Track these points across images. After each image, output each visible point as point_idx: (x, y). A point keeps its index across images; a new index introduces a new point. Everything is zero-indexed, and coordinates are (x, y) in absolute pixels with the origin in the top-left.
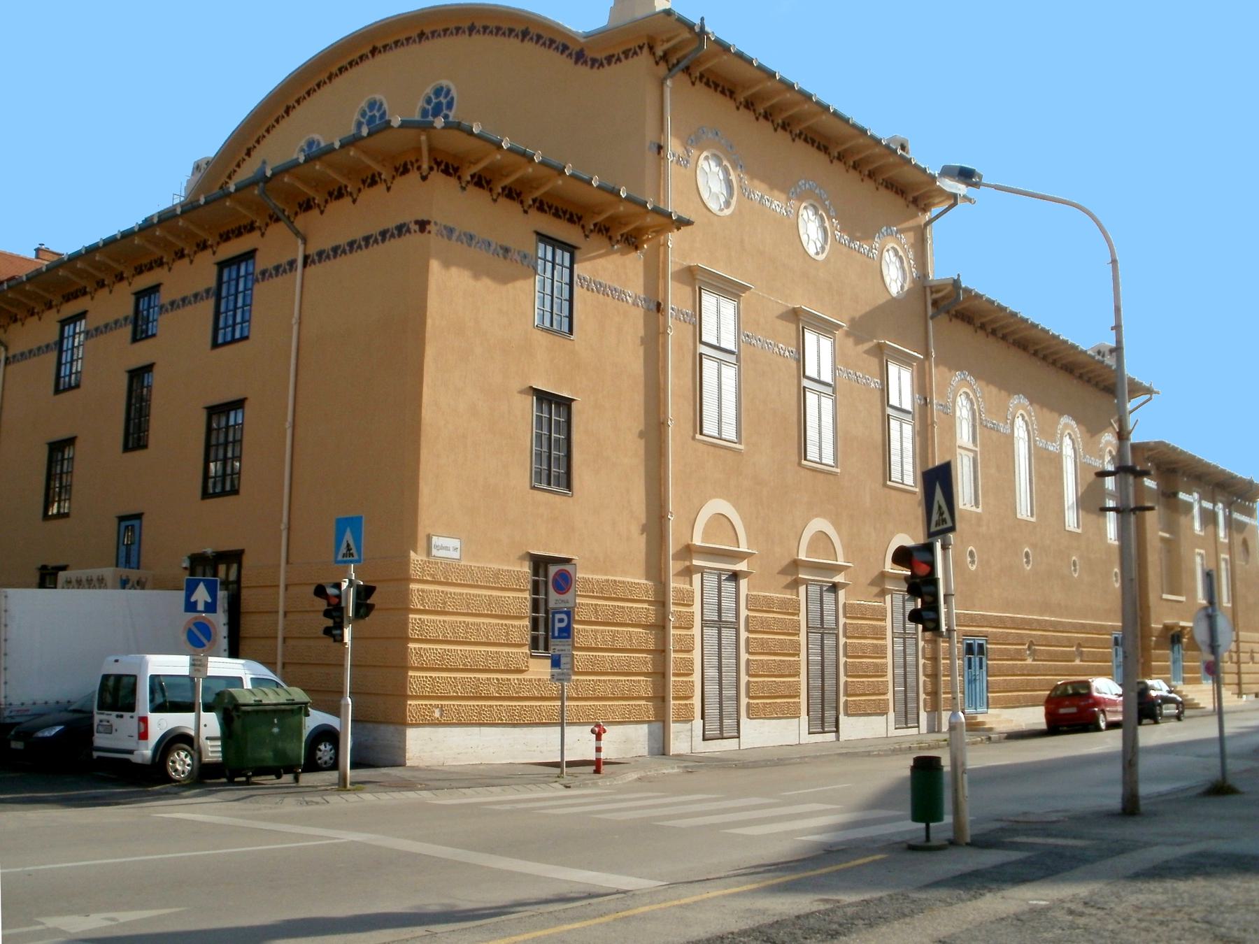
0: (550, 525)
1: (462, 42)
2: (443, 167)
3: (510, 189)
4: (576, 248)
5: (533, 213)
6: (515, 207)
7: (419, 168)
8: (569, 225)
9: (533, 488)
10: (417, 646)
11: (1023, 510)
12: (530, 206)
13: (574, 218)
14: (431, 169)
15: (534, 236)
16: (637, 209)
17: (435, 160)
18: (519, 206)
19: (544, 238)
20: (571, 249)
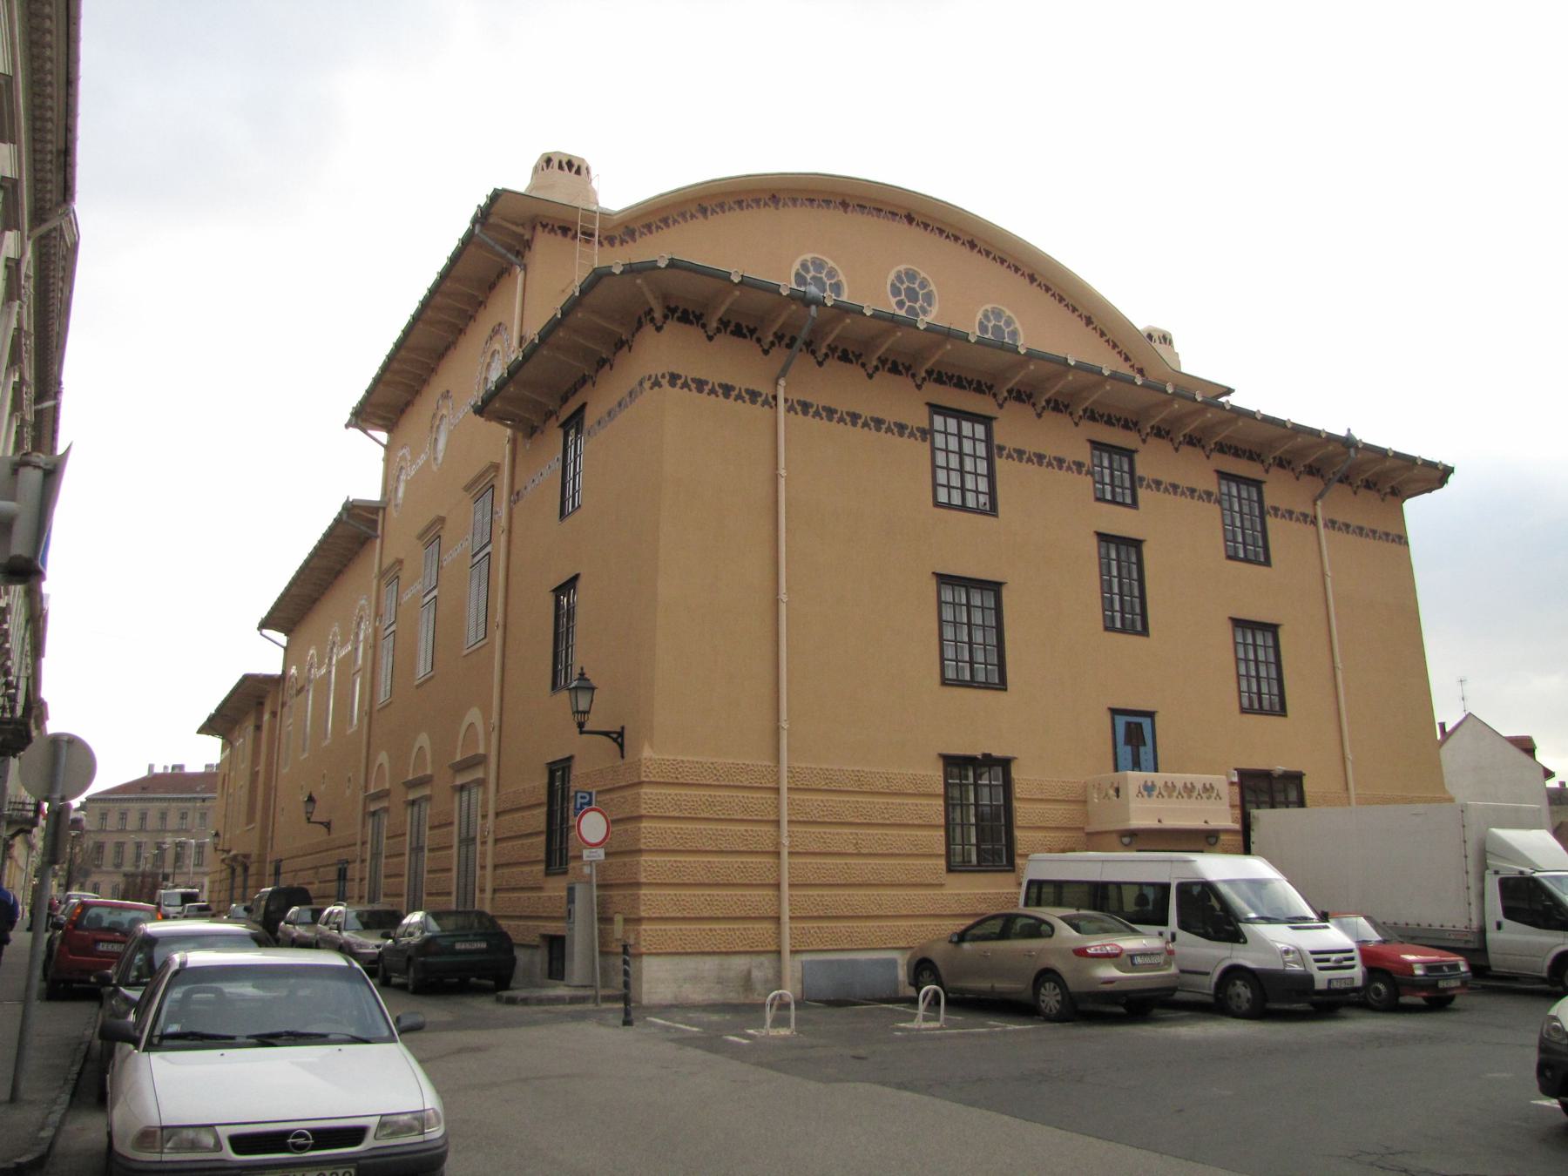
0: (978, 724)
1: (736, 217)
2: (889, 365)
3: (1019, 392)
4: (1261, 482)
5: (1085, 423)
6: (1063, 419)
7: (652, 320)
8: (978, 396)
9: (1151, 715)
10: (1029, 834)
11: (483, 945)
12: (924, 379)
13: (1253, 456)
14: (666, 317)
15: (1215, 476)
16: (1094, 378)
17: (668, 308)
18: (862, 371)
19: (935, 409)
20: (987, 421)
